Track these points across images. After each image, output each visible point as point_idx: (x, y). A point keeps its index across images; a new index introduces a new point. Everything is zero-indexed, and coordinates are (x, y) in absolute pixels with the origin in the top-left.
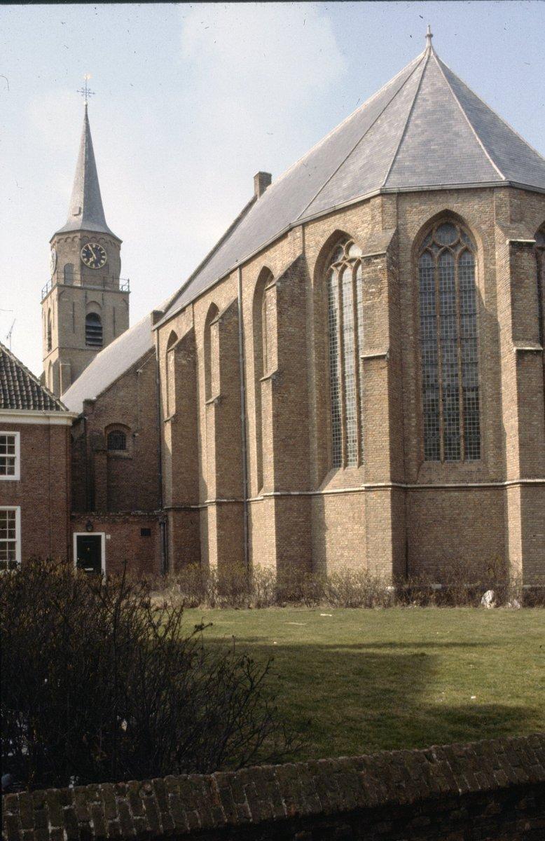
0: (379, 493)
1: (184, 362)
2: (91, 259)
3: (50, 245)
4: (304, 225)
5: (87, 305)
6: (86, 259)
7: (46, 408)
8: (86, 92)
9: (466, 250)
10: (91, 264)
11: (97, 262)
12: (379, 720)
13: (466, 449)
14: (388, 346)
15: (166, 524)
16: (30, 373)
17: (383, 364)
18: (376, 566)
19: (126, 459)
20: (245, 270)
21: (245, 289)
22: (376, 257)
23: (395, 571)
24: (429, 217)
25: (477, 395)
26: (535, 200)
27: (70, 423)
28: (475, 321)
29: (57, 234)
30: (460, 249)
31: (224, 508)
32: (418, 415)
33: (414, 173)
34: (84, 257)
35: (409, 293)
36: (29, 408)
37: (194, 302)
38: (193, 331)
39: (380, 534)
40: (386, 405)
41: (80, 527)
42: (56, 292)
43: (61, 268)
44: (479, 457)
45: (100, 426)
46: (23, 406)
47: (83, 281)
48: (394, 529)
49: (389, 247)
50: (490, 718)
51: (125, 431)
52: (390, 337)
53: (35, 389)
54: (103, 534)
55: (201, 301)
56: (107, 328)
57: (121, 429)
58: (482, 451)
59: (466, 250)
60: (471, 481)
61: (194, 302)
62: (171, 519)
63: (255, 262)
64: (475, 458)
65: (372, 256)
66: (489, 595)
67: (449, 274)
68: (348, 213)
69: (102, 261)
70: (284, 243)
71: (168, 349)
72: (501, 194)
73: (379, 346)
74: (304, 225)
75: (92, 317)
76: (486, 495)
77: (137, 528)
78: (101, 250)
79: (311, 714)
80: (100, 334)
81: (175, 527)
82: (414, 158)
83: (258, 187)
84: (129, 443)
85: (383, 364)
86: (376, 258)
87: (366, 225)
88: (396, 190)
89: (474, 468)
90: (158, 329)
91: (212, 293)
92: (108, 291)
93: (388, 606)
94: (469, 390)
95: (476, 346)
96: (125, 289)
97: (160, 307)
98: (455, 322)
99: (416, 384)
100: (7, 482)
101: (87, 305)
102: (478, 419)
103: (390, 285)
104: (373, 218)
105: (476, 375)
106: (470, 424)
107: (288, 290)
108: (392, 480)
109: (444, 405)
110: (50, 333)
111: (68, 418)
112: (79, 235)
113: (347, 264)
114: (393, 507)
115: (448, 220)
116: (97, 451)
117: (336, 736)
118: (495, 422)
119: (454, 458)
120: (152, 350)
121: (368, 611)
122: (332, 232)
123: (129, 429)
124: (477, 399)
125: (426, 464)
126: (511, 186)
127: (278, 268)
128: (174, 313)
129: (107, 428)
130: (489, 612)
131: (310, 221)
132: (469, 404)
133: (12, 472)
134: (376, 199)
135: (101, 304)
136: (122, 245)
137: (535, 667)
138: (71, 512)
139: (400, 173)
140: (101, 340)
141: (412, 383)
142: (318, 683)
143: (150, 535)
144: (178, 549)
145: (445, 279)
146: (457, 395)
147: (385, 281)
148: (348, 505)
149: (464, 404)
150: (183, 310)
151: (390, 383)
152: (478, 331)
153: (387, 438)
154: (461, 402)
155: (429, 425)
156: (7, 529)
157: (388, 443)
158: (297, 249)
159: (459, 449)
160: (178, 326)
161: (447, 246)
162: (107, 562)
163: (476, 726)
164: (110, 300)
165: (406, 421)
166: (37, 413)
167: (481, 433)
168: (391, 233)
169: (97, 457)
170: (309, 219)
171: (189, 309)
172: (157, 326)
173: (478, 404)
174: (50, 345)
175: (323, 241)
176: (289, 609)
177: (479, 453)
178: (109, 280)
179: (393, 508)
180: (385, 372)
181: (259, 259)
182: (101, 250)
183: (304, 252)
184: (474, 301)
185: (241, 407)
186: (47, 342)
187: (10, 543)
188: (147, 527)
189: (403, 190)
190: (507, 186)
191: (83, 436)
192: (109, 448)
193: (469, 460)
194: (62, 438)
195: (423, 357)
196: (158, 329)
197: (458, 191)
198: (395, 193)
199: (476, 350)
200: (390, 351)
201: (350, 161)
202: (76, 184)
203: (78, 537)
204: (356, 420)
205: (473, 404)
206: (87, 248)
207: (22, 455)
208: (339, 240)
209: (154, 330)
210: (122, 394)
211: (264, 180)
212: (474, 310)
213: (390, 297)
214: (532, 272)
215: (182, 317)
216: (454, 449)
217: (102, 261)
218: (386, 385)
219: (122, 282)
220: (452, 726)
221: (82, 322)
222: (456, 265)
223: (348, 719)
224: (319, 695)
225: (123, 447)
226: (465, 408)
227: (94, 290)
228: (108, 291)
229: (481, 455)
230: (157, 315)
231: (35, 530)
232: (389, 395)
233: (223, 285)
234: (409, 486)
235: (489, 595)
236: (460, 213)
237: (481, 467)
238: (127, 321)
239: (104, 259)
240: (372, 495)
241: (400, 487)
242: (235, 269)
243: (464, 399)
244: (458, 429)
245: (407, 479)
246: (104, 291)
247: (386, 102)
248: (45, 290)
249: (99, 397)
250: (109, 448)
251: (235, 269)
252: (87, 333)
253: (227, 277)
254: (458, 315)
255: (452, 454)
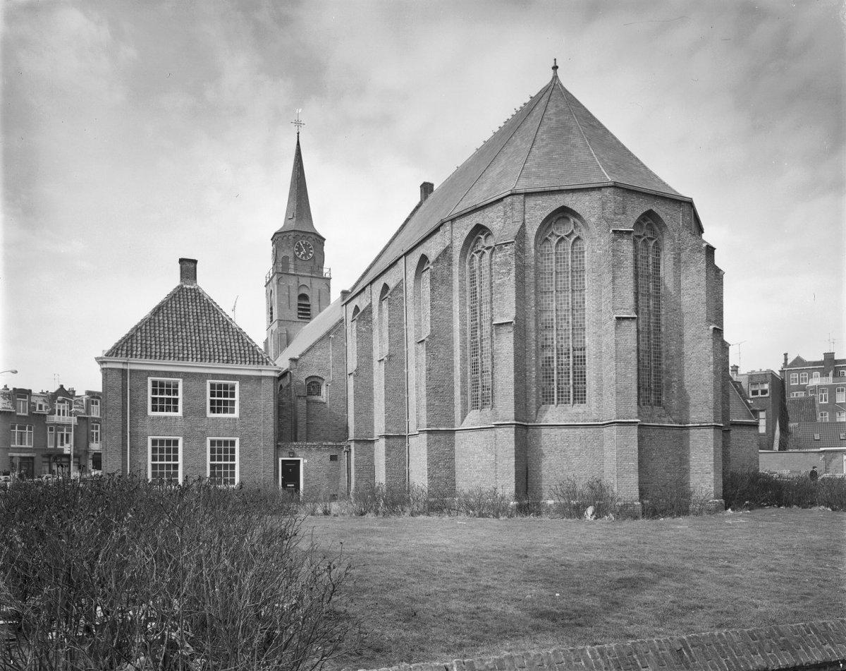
0: (506, 429)
1: (364, 329)
2: (302, 253)
3: (271, 242)
4: (453, 220)
5: (299, 288)
6: (298, 253)
7: (258, 362)
8: (298, 123)
9: (578, 238)
10: (302, 257)
11: (305, 255)
12: (473, 613)
13: (574, 395)
14: (515, 315)
15: (349, 452)
16: (248, 337)
17: (510, 328)
18: (502, 486)
19: (321, 403)
20: (409, 257)
21: (408, 272)
22: (506, 244)
23: (517, 490)
24: (550, 212)
25: (584, 353)
26: (635, 197)
27: (277, 375)
28: (584, 295)
29: (276, 234)
30: (573, 237)
31: (391, 441)
32: (537, 369)
33: (538, 177)
34: (297, 251)
35: (532, 273)
36: (155, 358)
37: (371, 283)
38: (370, 305)
39: (506, 461)
40: (512, 361)
41: (284, 454)
42: (275, 278)
43: (280, 259)
44: (585, 403)
45: (302, 377)
46: (201, 359)
47: (295, 269)
48: (516, 457)
49: (516, 237)
50: (567, 614)
51: (320, 381)
52: (516, 307)
53: (251, 349)
54: (301, 459)
55: (376, 282)
56: (313, 302)
57: (316, 380)
58: (587, 397)
59: (578, 238)
60: (578, 420)
61: (371, 283)
62: (353, 448)
63: (416, 251)
64: (582, 403)
65: (503, 244)
66: (590, 510)
67: (564, 258)
68: (486, 210)
69: (310, 255)
70: (437, 236)
71: (353, 317)
72: (608, 192)
73: (508, 315)
74: (453, 220)
75: (303, 297)
76: (590, 432)
77: (327, 455)
78: (309, 245)
79: (419, 606)
80: (309, 310)
81: (355, 454)
82: (539, 165)
83: (423, 194)
84: (324, 390)
85: (510, 328)
86: (506, 246)
87: (500, 219)
88: (523, 191)
89: (580, 411)
90: (346, 304)
91: (385, 276)
92: (314, 277)
93: (511, 516)
94: (578, 350)
95: (584, 314)
96: (327, 276)
97: (348, 288)
98: (568, 296)
99: (537, 345)
100: (230, 419)
101: (299, 288)
102: (585, 372)
103: (517, 266)
104: (505, 214)
105: (584, 337)
106: (578, 376)
107: (439, 272)
108: (516, 420)
109: (558, 361)
110: (271, 309)
111: (275, 371)
112: (292, 234)
113: (485, 251)
114: (516, 440)
115: (564, 213)
116: (299, 396)
117: (434, 626)
118: (598, 374)
119: (566, 403)
120: (341, 321)
121: (495, 521)
122: (473, 226)
123: (324, 380)
124: (584, 357)
125: (543, 407)
126: (615, 186)
127: (433, 255)
128: (358, 291)
129: (306, 379)
130: (590, 523)
131: (457, 217)
132: (578, 360)
133: (176, 410)
134: (508, 198)
135: (309, 287)
136: (325, 242)
137: (615, 570)
138: (277, 442)
139: (527, 178)
140: (309, 315)
141: (533, 344)
142: (434, 579)
143: (337, 460)
144: (358, 471)
145: (561, 262)
146: (569, 353)
147: (513, 263)
148: (483, 439)
149: (574, 361)
150: (363, 289)
151: (515, 344)
152: (586, 303)
153: (512, 387)
154: (571, 359)
155: (546, 377)
156: (216, 454)
157: (513, 391)
158: (446, 240)
159: (569, 396)
160: (360, 302)
161: (563, 235)
162: (304, 480)
163: (554, 620)
164: (317, 284)
165: (528, 374)
166: (252, 367)
167: (587, 383)
168: (518, 226)
169: (299, 401)
170: (456, 216)
171: (368, 289)
172: (345, 302)
173: (585, 360)
174: (271, 318)
175: (466, 233)
176: (434, 518)
177: (585, 399)
178: (316, 269)
179: (516, 440)
180: (512, 335)
181: (420, 248)
182: (309, 245)
183: (452, 242)
184: (584, 279)
185: (403, 363)
186: (269, 315)
187: (231, 465)
188: (334, 454)
189: (528, 191)
190: (612, 186)
191: (289, 385)
192: (308, 395)
193: (577, 404)
194: (270, 386)
195: (542, 324)
196: (346, 304)
197: (573, 191)
198: (522, 194)
199: (584, 318)
200: (516, 319)
201: (490, 169)
202: (290, 195)
203: (283, 461)
204: (490, 373)
205: (581, 361)
206: (299, 244)
207: (240, 398)
208: (480, 229)
209: (343, 306)
210: (318, 353)
211: (427, 188)
212: (584, 287)
213: (517, 276)
214: (630, 255)
215: (363, 295)
216: (566, 396)
217: (310, 255)
218: (512, 345)
219: (325, 271)
220: (533, 621)
221: (295, 301)
222: (570, 251)
223: (449, 611)
224: (431, 590)
225: (319, 394)
226: (574, 364)
227: (304, 276)
228: (314, 277)
229: (587, 401)
230: (344, 293)
231: (250, 456)
232: (515, 353)
233: (392, 269)
234: (529, 424)
235: (590, 510)
236: (574, 209)
237: (586, 410)
238: (329, 300)
239: (311, 253)
240: (499, 431)
241: (523, 425)
242: (401, 257)
243: (574, 357)
244: (569, 380)
245: (528, 419)
246: (312, 277)
247: (520, 122)
248: (268, 276)
249: (302, 355)
250: (308, 395)
251: (401, 257)
252: (299, 309)
253: (395, 263)
254: (570, 291)
255: (563, 399)
